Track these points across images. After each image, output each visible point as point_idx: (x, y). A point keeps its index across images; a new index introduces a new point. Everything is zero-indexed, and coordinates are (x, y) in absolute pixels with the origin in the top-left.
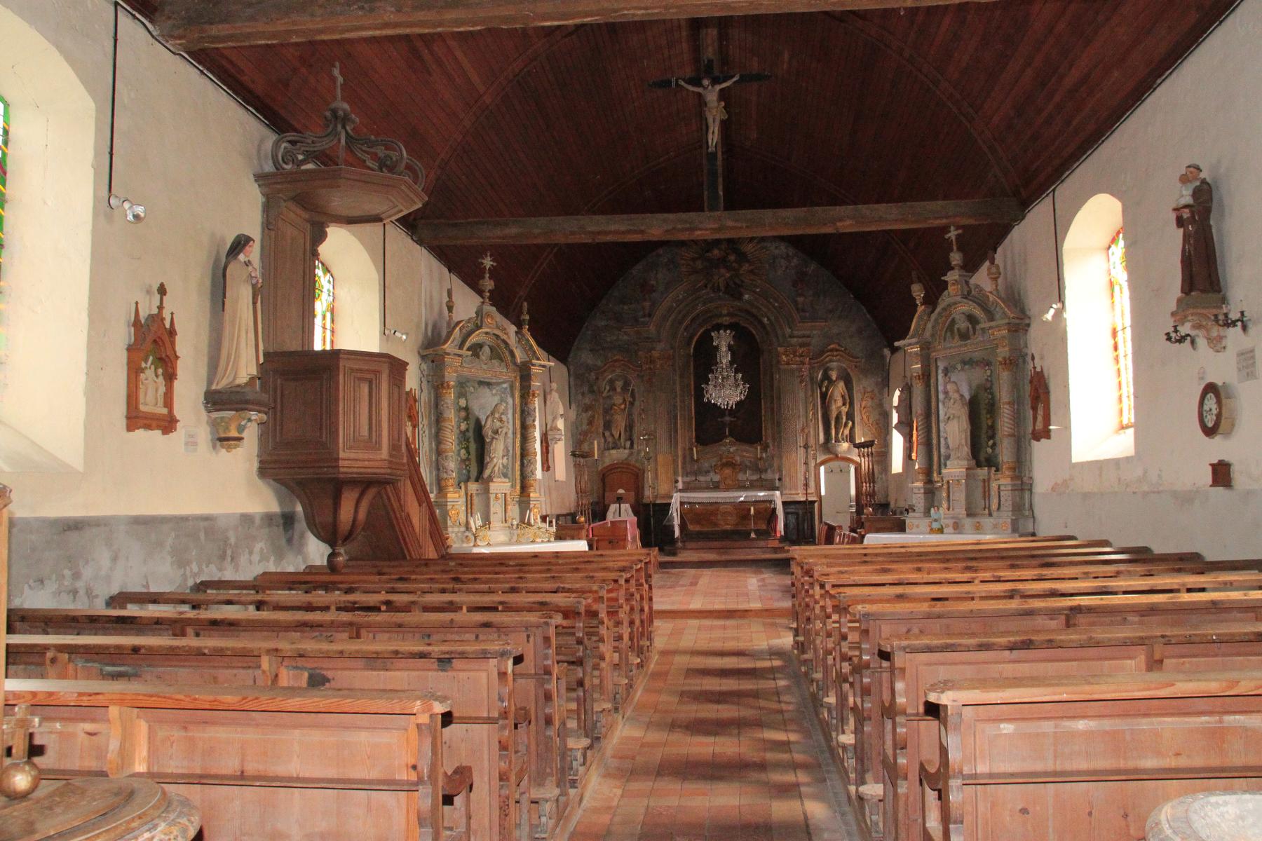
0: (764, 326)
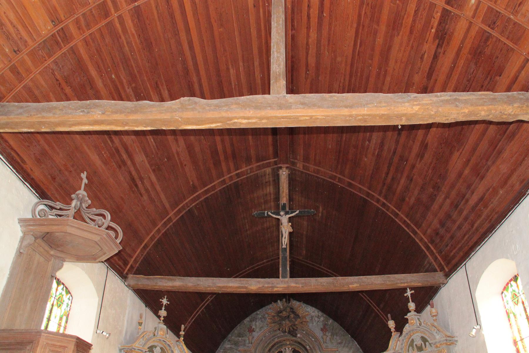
0: (306, 349)
